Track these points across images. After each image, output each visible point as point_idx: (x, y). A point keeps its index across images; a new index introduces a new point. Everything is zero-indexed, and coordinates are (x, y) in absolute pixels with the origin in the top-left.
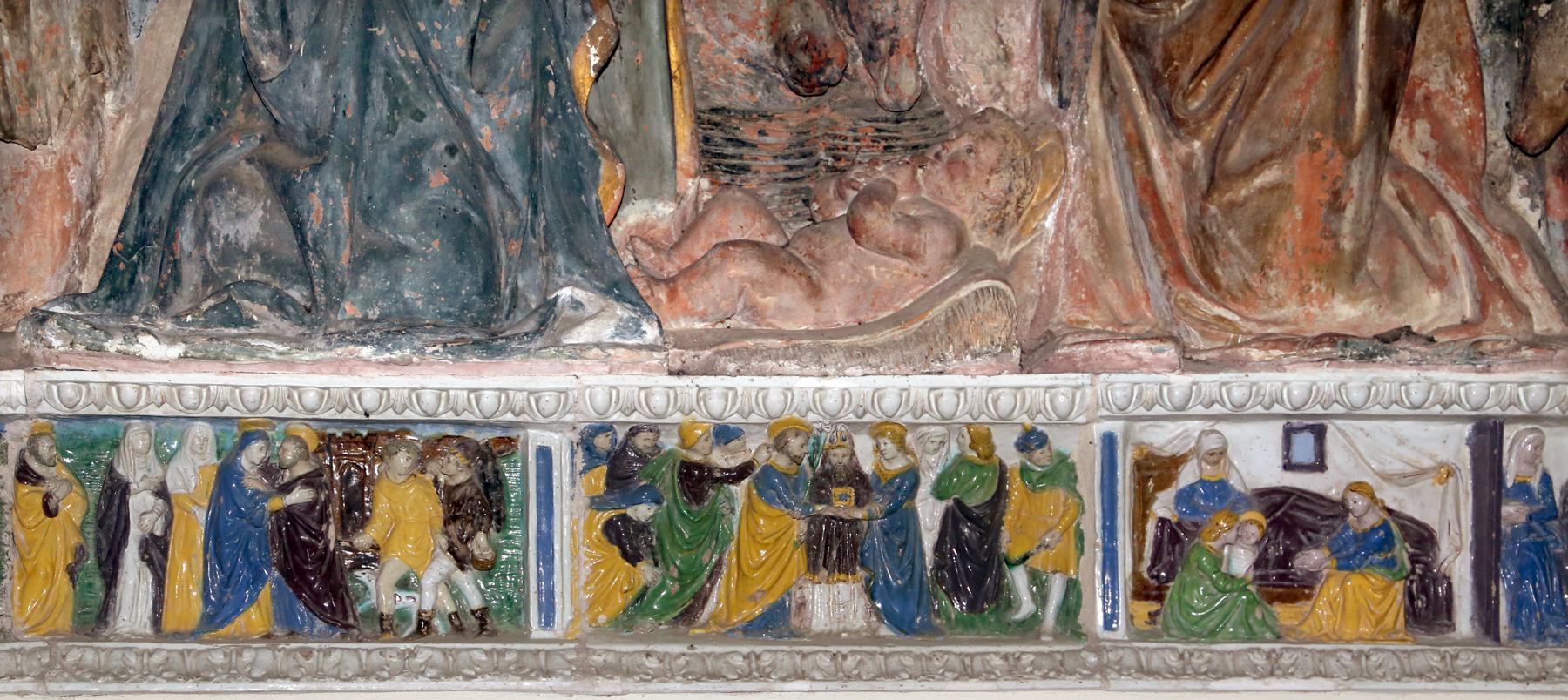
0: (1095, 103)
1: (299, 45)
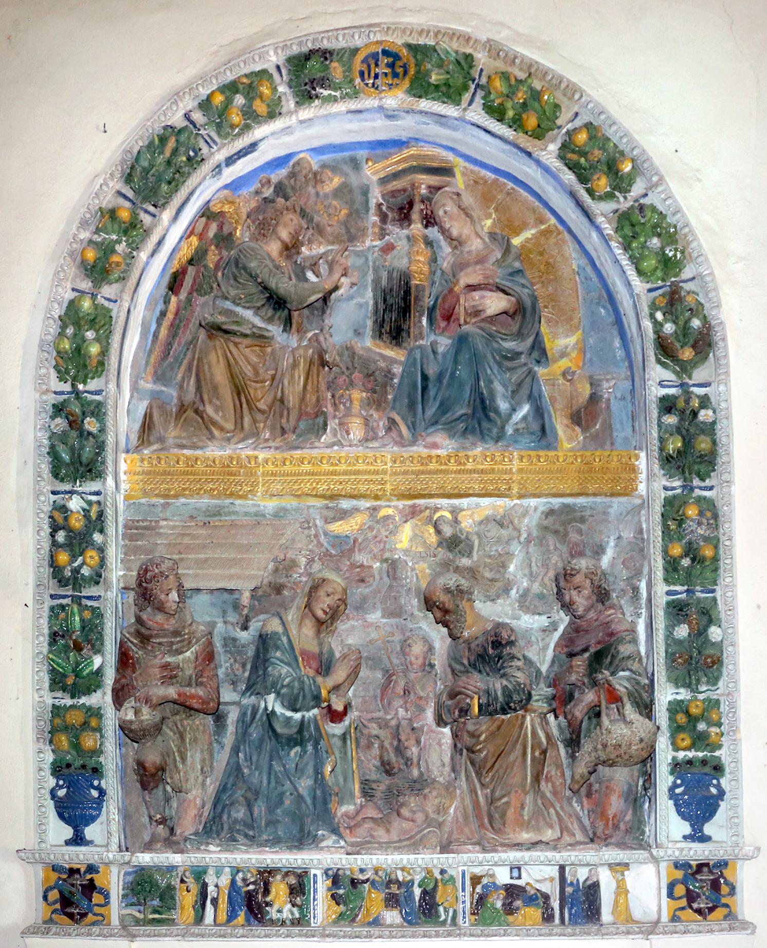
0: (464, 779)
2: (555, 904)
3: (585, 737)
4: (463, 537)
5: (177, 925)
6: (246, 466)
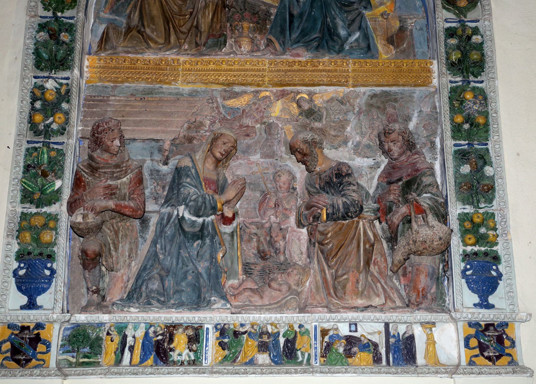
0: (316, 263)
1: (167, 254)
2: (383, 350)
3: (401, 236)
4: (316, 110)
5: (101, 366)
6: (171, 65)
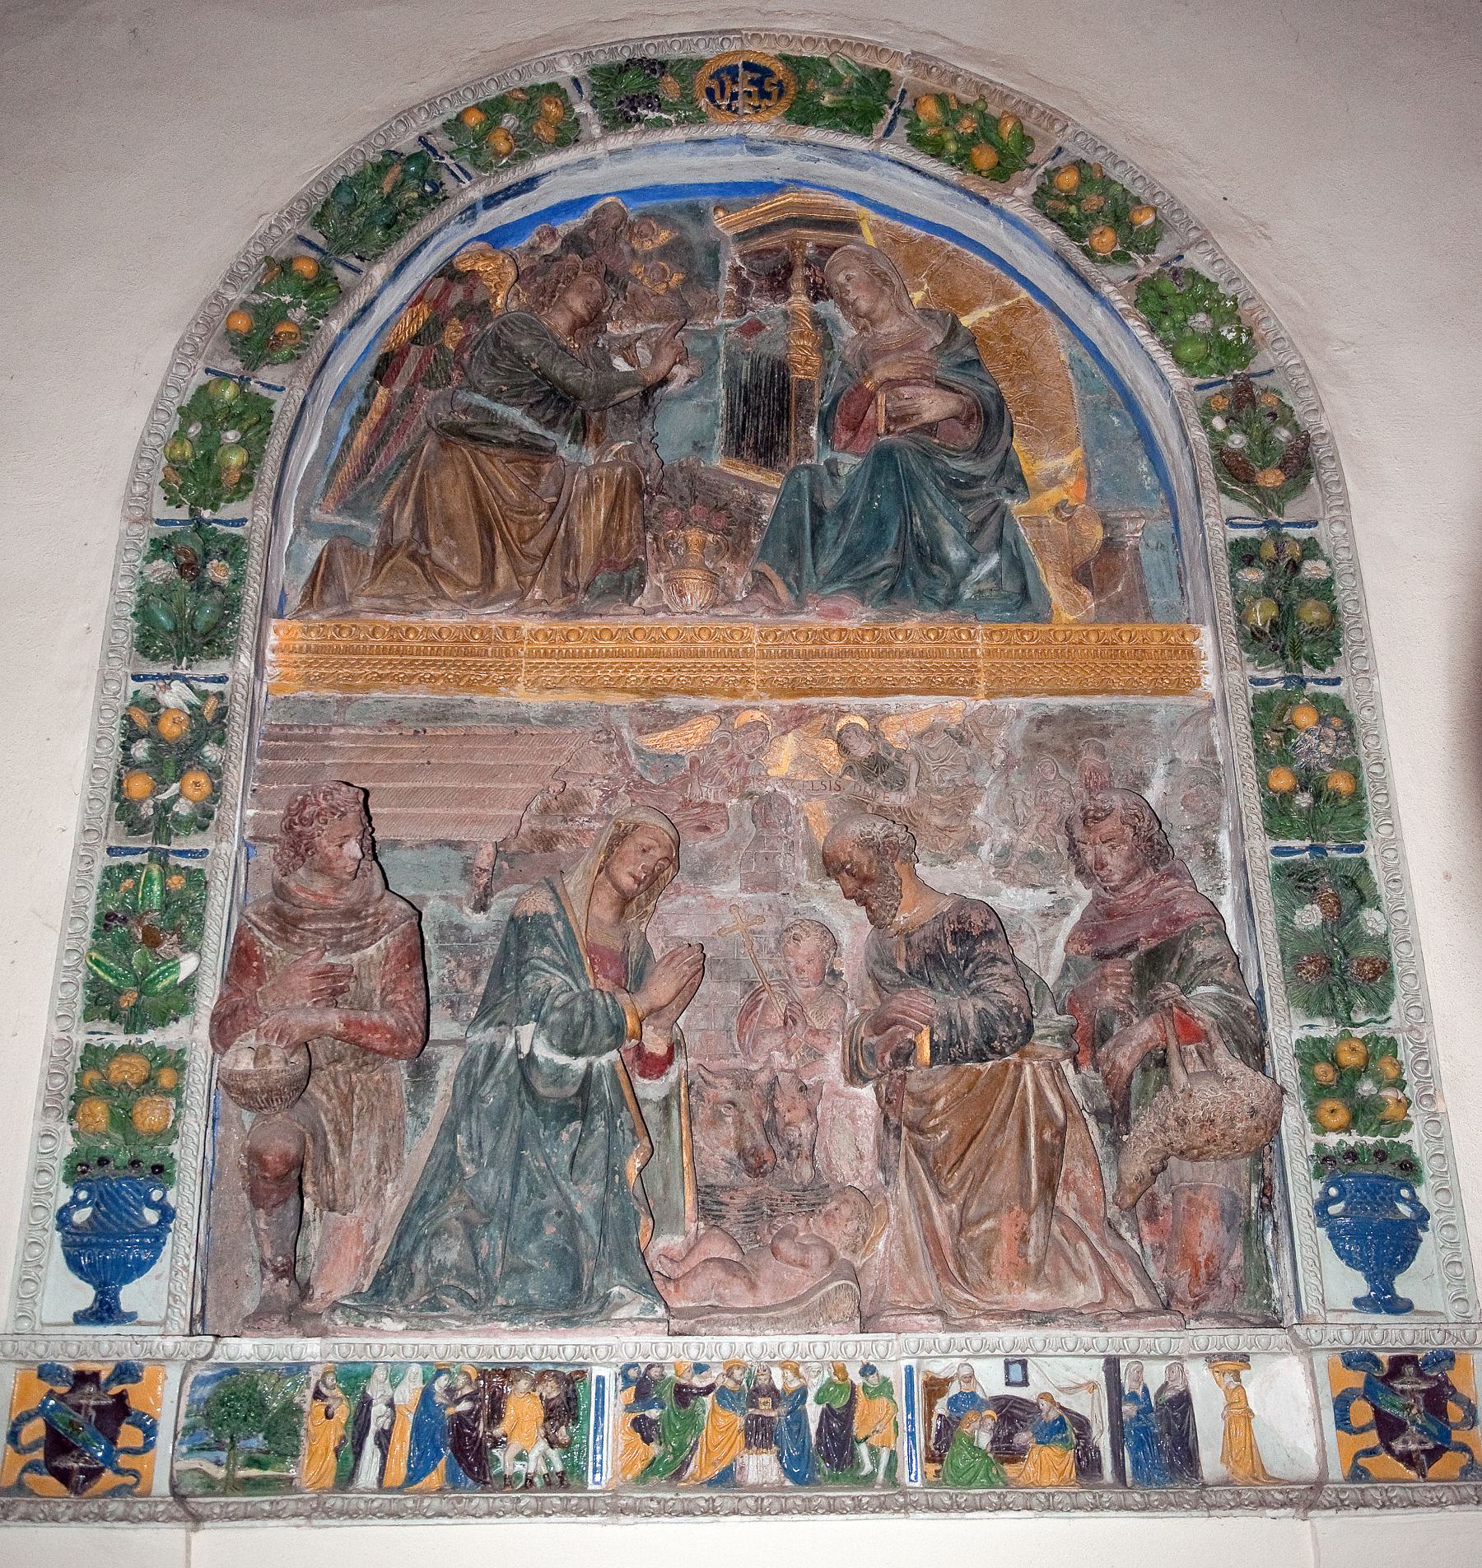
0: (903, 1183)
5: (298, 1491)
